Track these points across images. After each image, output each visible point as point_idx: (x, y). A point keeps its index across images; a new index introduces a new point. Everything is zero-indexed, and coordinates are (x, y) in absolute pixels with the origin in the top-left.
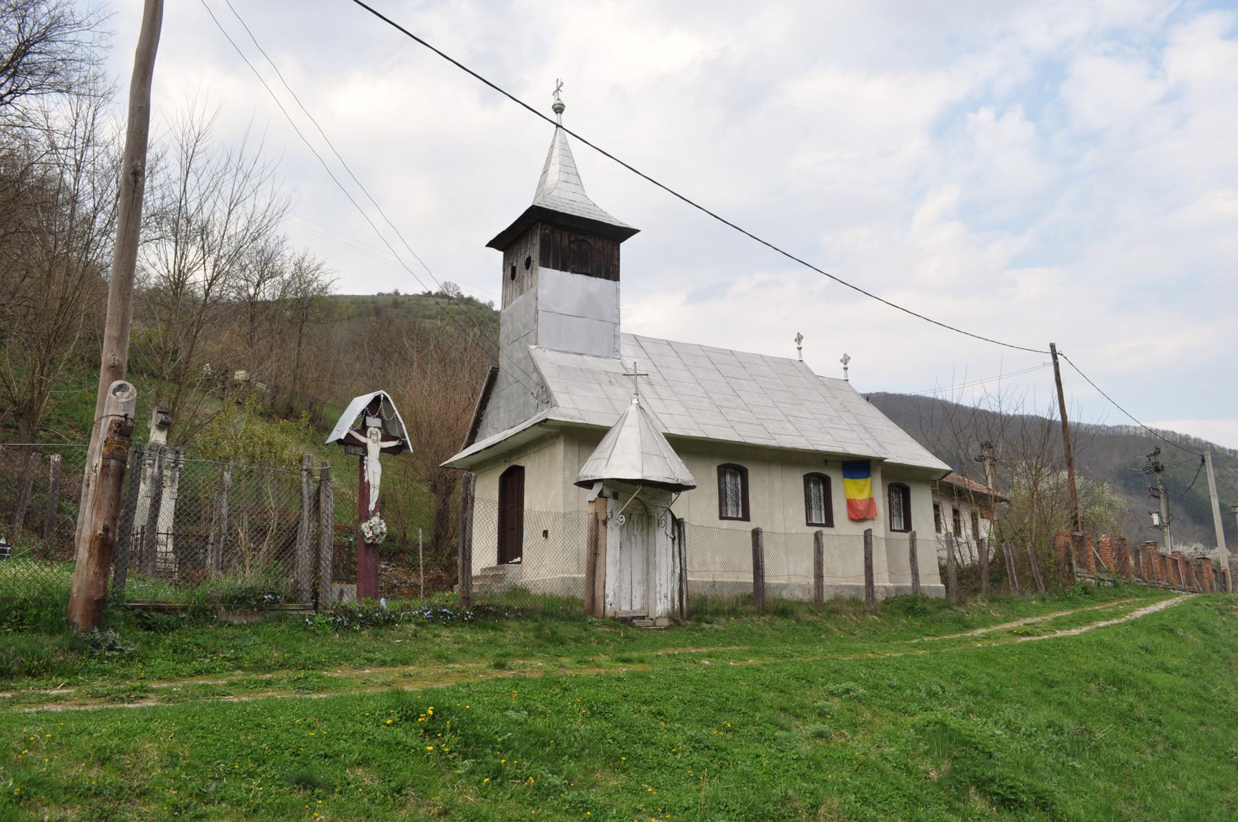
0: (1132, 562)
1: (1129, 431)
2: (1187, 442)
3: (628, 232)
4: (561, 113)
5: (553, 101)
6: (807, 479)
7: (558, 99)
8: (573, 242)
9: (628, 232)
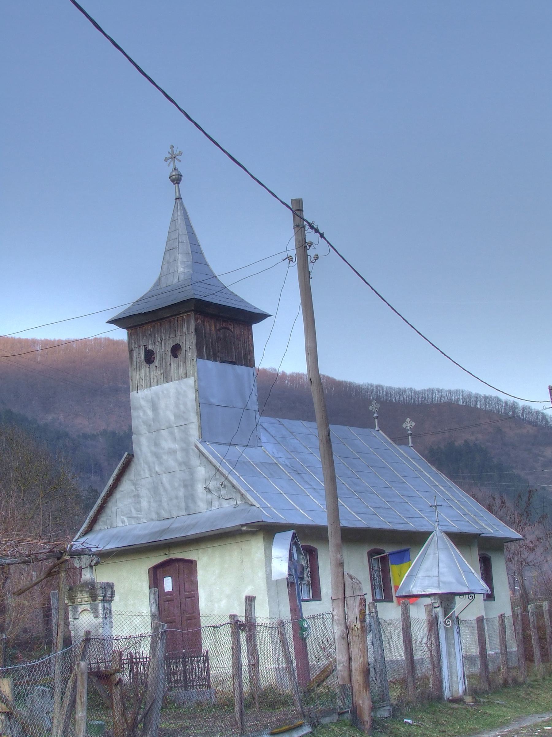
0: (188, 667)
1: (442, 397)
2: (514, 412)
3: (260, 317)
4: (178, 183)
5: (168, 170)
6: (371, 554)
7: (175, 169)
8: (219, 330)
9: (260, 317)
